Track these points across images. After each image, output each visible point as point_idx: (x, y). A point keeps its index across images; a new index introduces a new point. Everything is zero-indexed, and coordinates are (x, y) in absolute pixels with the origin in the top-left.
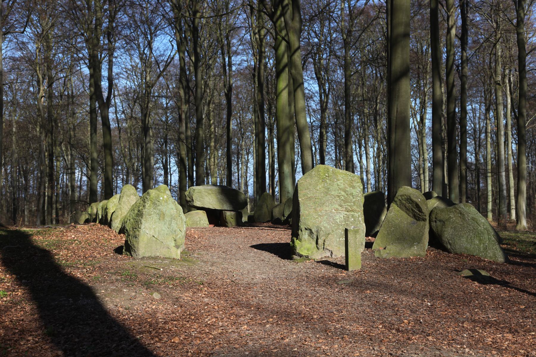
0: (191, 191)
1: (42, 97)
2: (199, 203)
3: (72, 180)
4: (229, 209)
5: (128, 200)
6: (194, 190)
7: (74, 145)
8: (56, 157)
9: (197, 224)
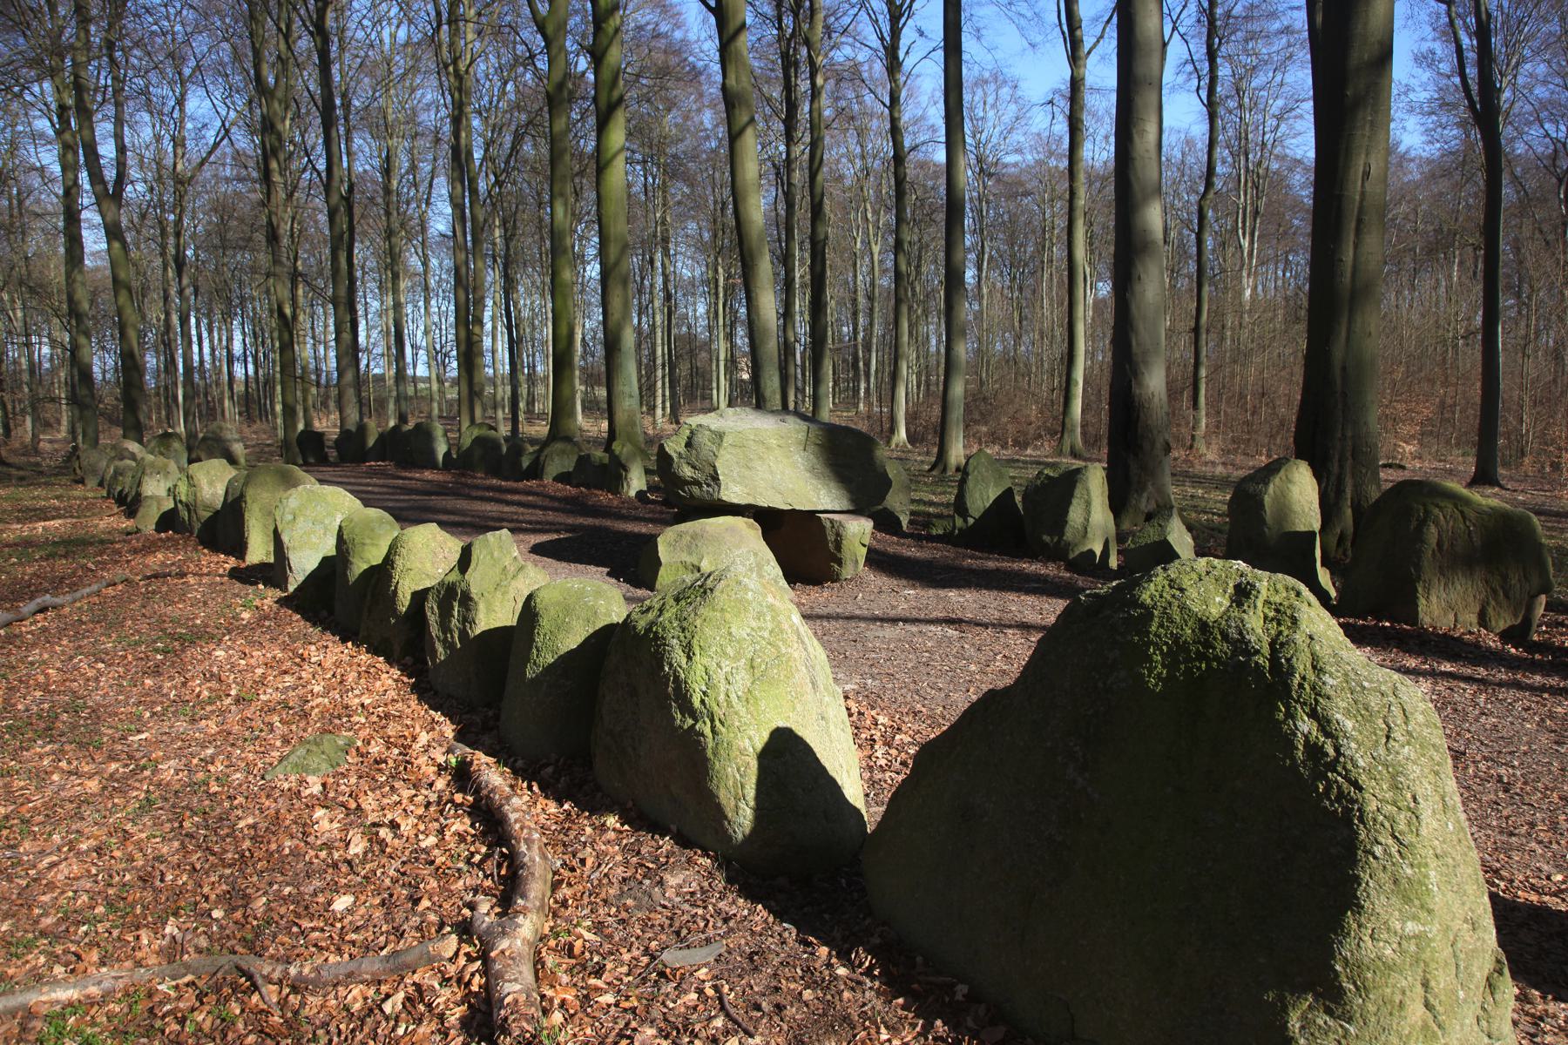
0: (703, 439)
2: (737, 489)
6: (720, 436)
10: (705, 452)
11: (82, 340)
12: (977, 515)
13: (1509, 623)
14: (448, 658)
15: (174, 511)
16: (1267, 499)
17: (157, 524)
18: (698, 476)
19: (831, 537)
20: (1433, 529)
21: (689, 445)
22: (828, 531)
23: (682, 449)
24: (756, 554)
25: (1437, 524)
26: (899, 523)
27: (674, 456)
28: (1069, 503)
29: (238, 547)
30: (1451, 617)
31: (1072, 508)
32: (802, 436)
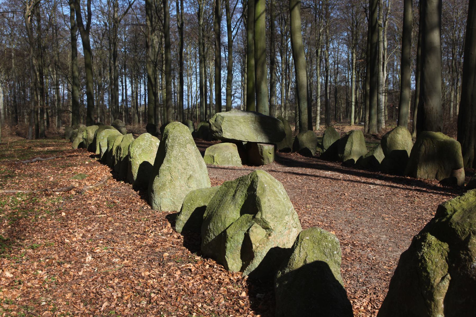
0: (219, 119)
1: (28, 17)
2: (229, 134)
3: (58, 92)
4: (264, 142)
5: (183, 153)
6: (223, 118)
7: (59, 66)
8: (45, 76)
9: (229, 162)
10: (219, 122)
11: (75, 88)
12: (327, 149)
13: (444, 178)
14: (281, 276)
15: (83, 142)
16: (388, 139)
17: (78, 146)
18: (217, 130)
19: (260, 151)
20: (423, 147)
21: (215, 121)
22: (259, 149)
23: (214, 122)
24: (231, 154)
25: (425, 145)
26: (311, 153)
27: (212, 124)
28: (346, 143)
29: (94, 151)
30: (427, 175)
31: (347, 145)
32: (253, 119)
